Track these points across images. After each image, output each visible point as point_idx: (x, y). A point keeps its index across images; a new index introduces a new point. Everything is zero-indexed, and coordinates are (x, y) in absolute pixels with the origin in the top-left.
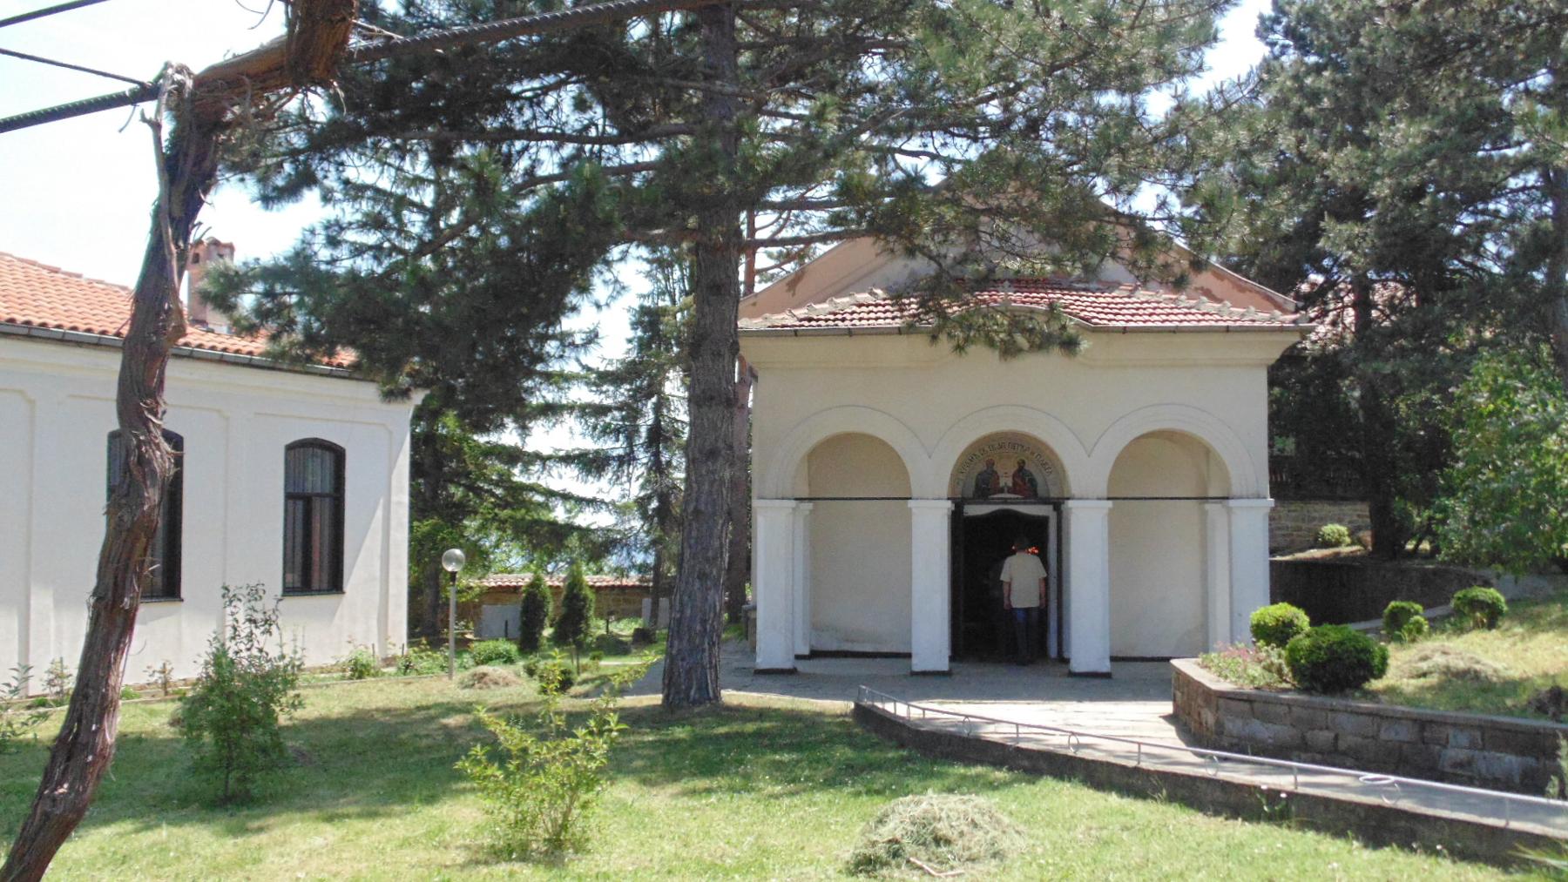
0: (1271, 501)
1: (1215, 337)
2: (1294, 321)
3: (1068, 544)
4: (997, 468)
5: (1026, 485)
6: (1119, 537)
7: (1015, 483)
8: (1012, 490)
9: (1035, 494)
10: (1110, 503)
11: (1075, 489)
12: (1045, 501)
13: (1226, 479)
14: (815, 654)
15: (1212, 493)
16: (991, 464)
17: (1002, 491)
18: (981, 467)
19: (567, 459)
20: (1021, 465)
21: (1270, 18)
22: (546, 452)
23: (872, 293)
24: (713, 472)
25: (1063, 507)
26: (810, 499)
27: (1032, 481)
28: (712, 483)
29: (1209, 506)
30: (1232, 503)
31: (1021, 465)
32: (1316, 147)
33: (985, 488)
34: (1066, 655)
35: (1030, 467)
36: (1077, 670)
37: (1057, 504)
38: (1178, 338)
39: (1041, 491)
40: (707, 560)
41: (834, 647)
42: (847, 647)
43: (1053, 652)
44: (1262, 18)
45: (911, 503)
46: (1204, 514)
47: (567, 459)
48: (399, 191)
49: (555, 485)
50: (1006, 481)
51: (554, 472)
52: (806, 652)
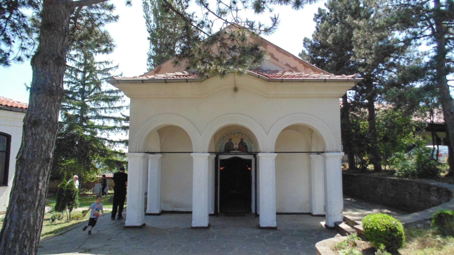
0: (343, 154)
1: (318, 85)
2: (353, 77)
3: (259, 175)
4: (233, 141)
5: (243, 148)
6: (280, 170)
7: (239, 147)
8: (238, 150)
9: (247, 151)
10: (276, 154)
11: (261, 148)
12: (250, 153)
13: (324, 145)
14: (163, 212)
15: (312, 151)
16: (230, 140)
17: (234, 150)
18: (227, 141)
19: (120, 142)
20: (242, 140)
21: (317, 15)
22: (114, 140)
23: (183, 73)
24: (35, 134)
25: (257, 156)
26: (161, 153)
27: (246, 146)
28: (34, 142)
29: (312, 156)
30: (327, 154)
31: (242, 140)
32: (352, 19)
33: (228, 149)
34: (258, 213)
35: (245, 141)
36: (262, 226)
37: (255, 155)
38: (305, 85)
39: (249, 150)
40: (25, 191)
41: (170, 209)
42: (175, 209)
43: (253, 211)
44: (315, 15)
45: (192, 154)
46: (310, 159)
47: (120, 142)
48: (77, 68)
49: (118, 149)
50: (236, 146)
51: (117, 146)
52: (157, 212)
